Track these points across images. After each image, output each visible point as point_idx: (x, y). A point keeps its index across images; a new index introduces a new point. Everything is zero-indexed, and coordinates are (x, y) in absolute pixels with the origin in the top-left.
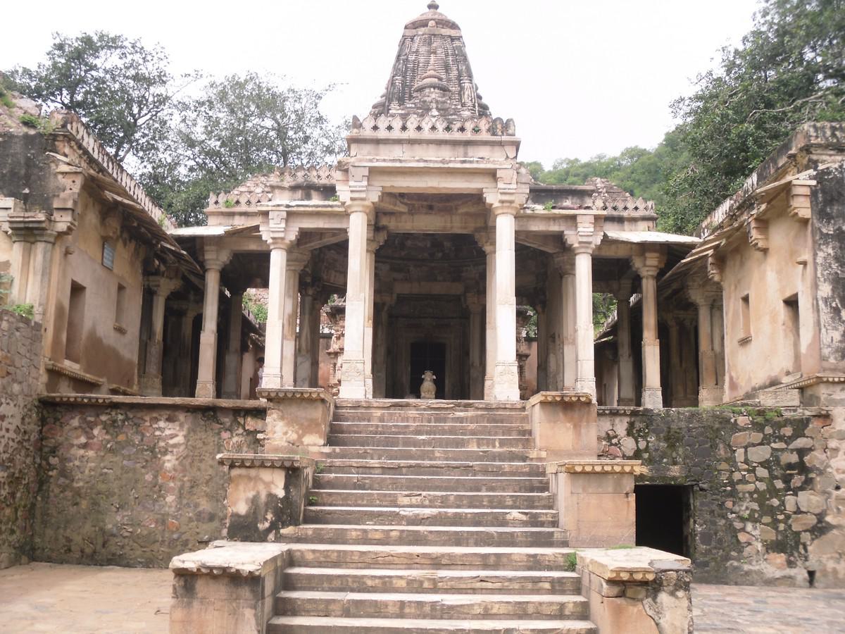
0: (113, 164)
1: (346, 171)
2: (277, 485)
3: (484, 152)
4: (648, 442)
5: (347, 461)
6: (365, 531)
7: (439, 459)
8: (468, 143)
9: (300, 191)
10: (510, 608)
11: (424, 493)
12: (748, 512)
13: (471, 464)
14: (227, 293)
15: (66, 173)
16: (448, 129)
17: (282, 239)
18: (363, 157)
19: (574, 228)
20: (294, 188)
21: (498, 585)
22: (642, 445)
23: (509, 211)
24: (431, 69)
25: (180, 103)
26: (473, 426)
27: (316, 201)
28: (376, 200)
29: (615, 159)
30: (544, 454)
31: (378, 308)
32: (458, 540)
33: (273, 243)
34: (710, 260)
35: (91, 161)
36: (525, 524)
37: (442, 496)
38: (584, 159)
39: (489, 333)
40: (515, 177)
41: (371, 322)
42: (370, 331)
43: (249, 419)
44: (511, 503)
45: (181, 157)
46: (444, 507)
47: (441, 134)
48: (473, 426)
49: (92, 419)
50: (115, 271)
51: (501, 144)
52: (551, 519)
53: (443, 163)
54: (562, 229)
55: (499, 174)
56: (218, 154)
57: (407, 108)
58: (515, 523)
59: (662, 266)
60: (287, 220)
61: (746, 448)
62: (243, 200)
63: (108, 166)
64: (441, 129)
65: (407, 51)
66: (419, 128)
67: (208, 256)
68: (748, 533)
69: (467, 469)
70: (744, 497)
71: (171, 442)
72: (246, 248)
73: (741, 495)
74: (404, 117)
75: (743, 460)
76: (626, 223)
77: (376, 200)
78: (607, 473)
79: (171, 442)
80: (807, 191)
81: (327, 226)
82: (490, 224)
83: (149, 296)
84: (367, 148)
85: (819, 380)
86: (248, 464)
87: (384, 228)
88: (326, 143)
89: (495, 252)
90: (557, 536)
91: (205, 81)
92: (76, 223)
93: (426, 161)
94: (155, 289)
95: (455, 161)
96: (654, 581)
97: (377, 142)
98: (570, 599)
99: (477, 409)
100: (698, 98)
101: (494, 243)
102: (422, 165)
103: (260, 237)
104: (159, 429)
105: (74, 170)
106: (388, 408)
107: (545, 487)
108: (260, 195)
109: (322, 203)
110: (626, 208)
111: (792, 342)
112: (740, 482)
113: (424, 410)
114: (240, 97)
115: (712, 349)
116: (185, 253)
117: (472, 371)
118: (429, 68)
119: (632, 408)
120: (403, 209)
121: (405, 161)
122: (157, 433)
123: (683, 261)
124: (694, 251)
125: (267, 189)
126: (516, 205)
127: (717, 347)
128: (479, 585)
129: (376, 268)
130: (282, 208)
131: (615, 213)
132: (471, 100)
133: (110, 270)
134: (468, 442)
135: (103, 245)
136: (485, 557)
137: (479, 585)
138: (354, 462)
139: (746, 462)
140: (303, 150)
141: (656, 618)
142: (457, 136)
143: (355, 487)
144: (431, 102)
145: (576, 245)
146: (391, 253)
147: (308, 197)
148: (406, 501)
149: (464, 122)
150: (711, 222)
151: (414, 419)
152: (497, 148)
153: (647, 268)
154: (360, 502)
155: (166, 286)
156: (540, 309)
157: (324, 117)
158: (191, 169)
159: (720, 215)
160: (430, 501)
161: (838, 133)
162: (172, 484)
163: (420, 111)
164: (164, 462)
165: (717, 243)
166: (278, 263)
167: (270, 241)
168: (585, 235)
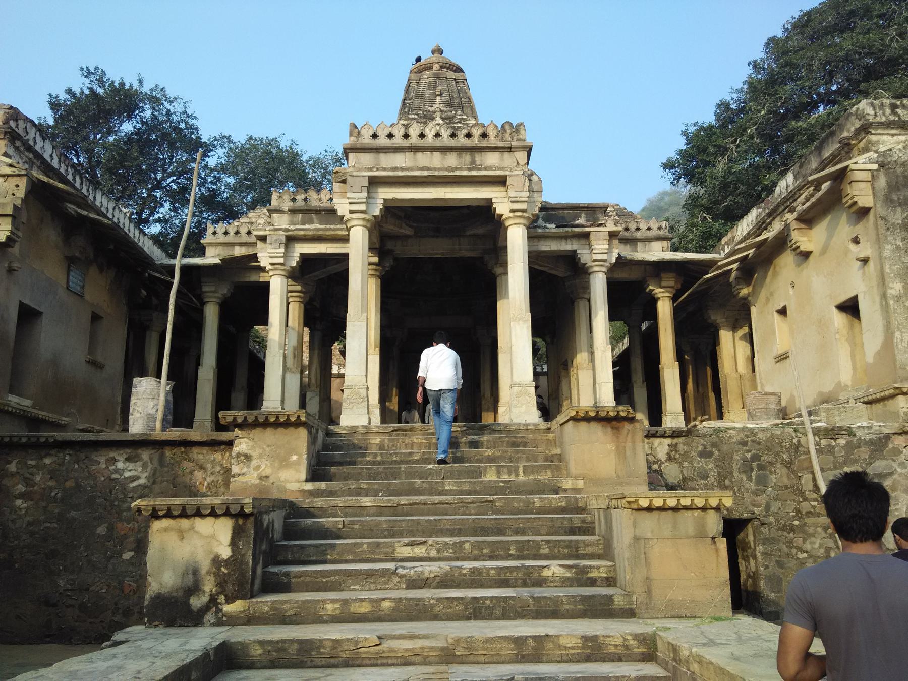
0: (81, 178)
3: (491, 159)
6: (345, 602)
11: (430, 541)
13: (490, 498)
15: (8, 176)
16: (453, 135)
18: (360, 166)
19: (587, 247)
20: (293, 212)
27: (315, 227)
30: (580, 484)
32: (477, 611)
34: (734, 275)
35: (47, 168)
36: (566, 582)
37: (455, 544)
40: (527, 184)
41: (378, 349)
46: (457, 559)
49: (33, 463)
50: (87, 297)
51: (509, 149)
52: (605, 575)
53: (449, 171)
54: (575, 248)
59: (679, 286)
60: (287, 247)
62: (243, 230)
63: (74, 179)
66: (422, 136)
67: (205, 289)
70: (816, 532)
73: (811, 530)
80: (867, 176)
82: (500, 244)
84: (366, 159)
85: (898, 391)
86: (176, 513)
87: (390, 252)
89: (506, 273)
90: (619, 601)
92: (20, 234)
101: (505, 264)
104: (117, 471)
105: (17, 172)
107: (587, 529)
110: (638, 229)
111: (849, 353)
112: (809, 514)
117: (483, 402)
120: (409, 231)
122: (115, 476)
133: (81, 296)
134: (486, 471)
135: (69, 267)
136: (519, 641)
138: (340, 502)
142: (462, 141)
145: (589, 264)
152: (506, 155)
156: (549, 340)
159: (745, 226)
161: (899, 111)
165: (745, 254)
166: (278, 286)
168: (599, 253)
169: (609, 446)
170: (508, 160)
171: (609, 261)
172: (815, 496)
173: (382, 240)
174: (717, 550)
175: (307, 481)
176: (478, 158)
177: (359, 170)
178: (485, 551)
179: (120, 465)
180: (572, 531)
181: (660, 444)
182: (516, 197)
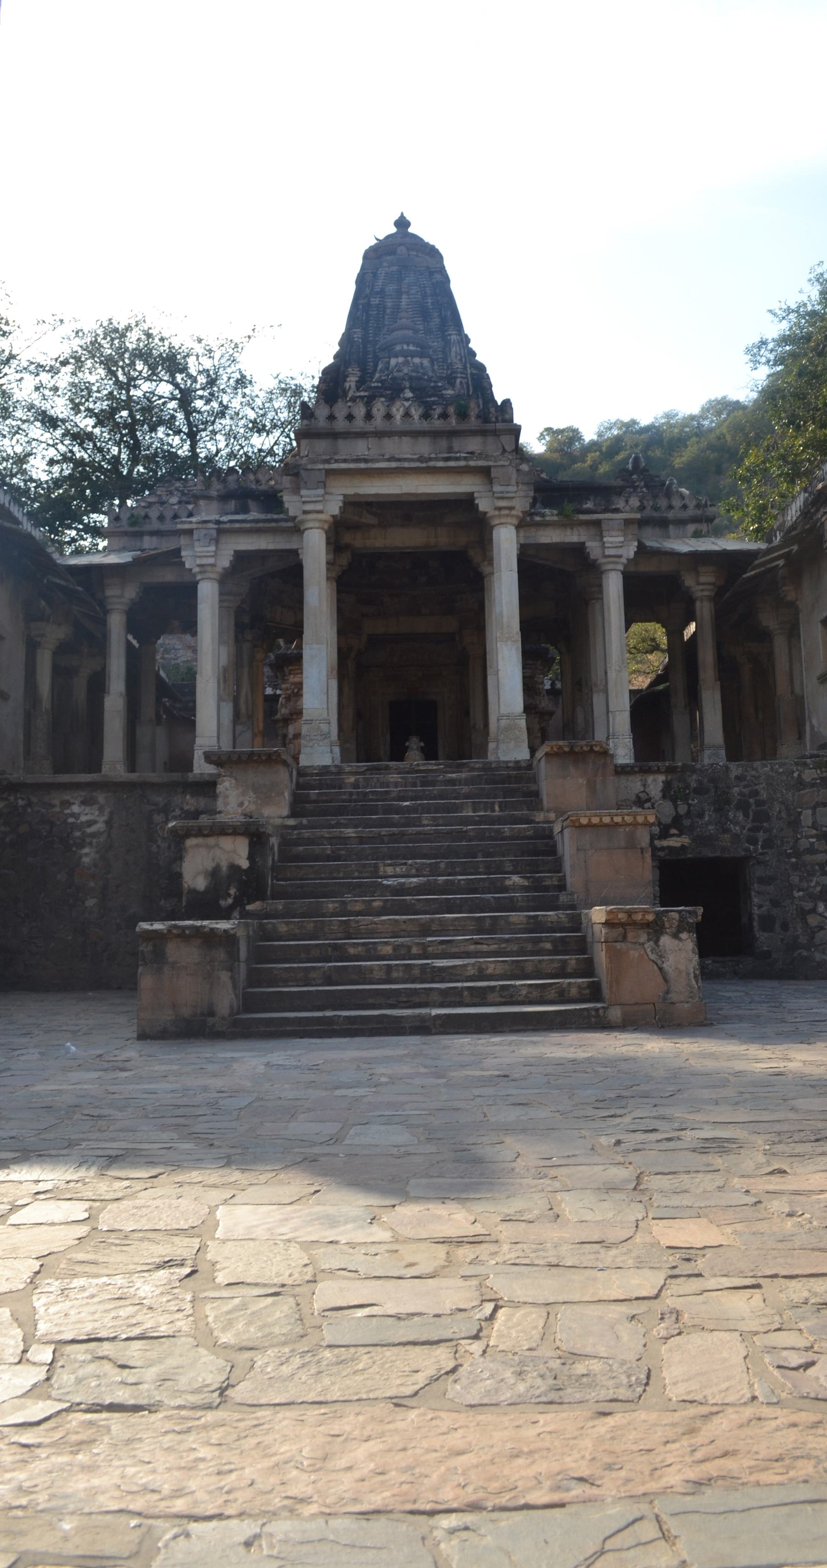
1: (297, 475)
2: (238, 852)
4: (689, 805)
5: (318, 832)
7: (427, 825)
8: (452, 434)
9: (233, 502)
10: (507, 967)
11: (410, 862)
12: (819, 889)
14: (135, 643)
17: (213, 565)
19: (598, 538)
21: (494, 947)
22: (683, 809)
23: (509, 520)
24: (403, 286)
25: (32, 363)
26: (465, 789)
28: (336, 512)
29: (692, 418)
31: (343, 654)
33: (201, 572)
37: (431, 864)
38: (645, 420)
39: (491, 680)
42: (334, 684)
43: (188, 797)
44: (511, 869)
45: (34, 444)
47: (417, 422)
48: (465, 789)
53: (422, 462)
54: (582, 539)
55: (494, 473)
56: (90, 436)
57: (371, 388)
58: (515, 888)
61: (814, 808)
64: (416, 417)
65: (368, 291)
67: (109, 592)
68: (820, 915)
69: (461, 835)
71: (89, 830)
72: (161, 580)
74: (369, 402)
75: (810, 824)
76: (671, 527)
77: (336, 512)
78: (617, 824)
79: (89, 830)
81: (271, 547)
83: (32, 646)
86: (206, 832)
87: (348, 547)
88: (252, 415)
89: (493, 573)
91: (67, 329)
93: (399, 460)
94: (39, 639)
95: (436, 459)
96: (655, 922)
97: (334, 436)
98: (572, 960)
99: (473, 769)
100: (784, 340)
101: (491, 562)
102: (393, 465)
103: (183, 564)
104: (73, 815)
106: (363, 773)
108: (176, 507)
109: (262, 516)
113: (408, 773)
114: (121, 351)
115: (793, 692)
116: (80, 589)
118: (400, 315)
119: (667, 764)
120: (371, 520)
121: (372, 461)
122: (71, 820)
123: (745, 576)
124: (756, 562)
125: (184, 498)
126: (517, 512)
127: (797, 690)
128: (472, 948)
129: (338, 601)
130: (211, 525)
131: (656, 514)
132: (461, 360)
137: (472, 948)
138: (325, 833)
139: (814, 826)
140: (217, 427)
141: (659, 962)
142: (438, 424)
143: (328, 858)
144: (403, 379)
146: (356, 576)
147: (245, 510)
148: (390, 870)
149: (446, 406)
150: (784, 522)
151: (396, 785)
152: (490, 439)
153: (701, 585)
154: (335, 875)
155: (55, 633)
157: (249, 378)
158: (52, 462)
160: (417, 870)
162: (92, 884)
163: (389, 392)
164: (81, 857)
166: (208, 593)
167: (196, 570)
168: (615, 548)
169: (580, 781)
170: (491, 446)
171: (625, 555)
172: (814, 832)
173: (338, 533)
174: (643, 858)
175: (288, 817)
176: (457, 444)
177: (314, 462)
178: (457, 869)
179: (76, 809)
180: (536, 853)
181: (654, 780)
182: (502, 492)
